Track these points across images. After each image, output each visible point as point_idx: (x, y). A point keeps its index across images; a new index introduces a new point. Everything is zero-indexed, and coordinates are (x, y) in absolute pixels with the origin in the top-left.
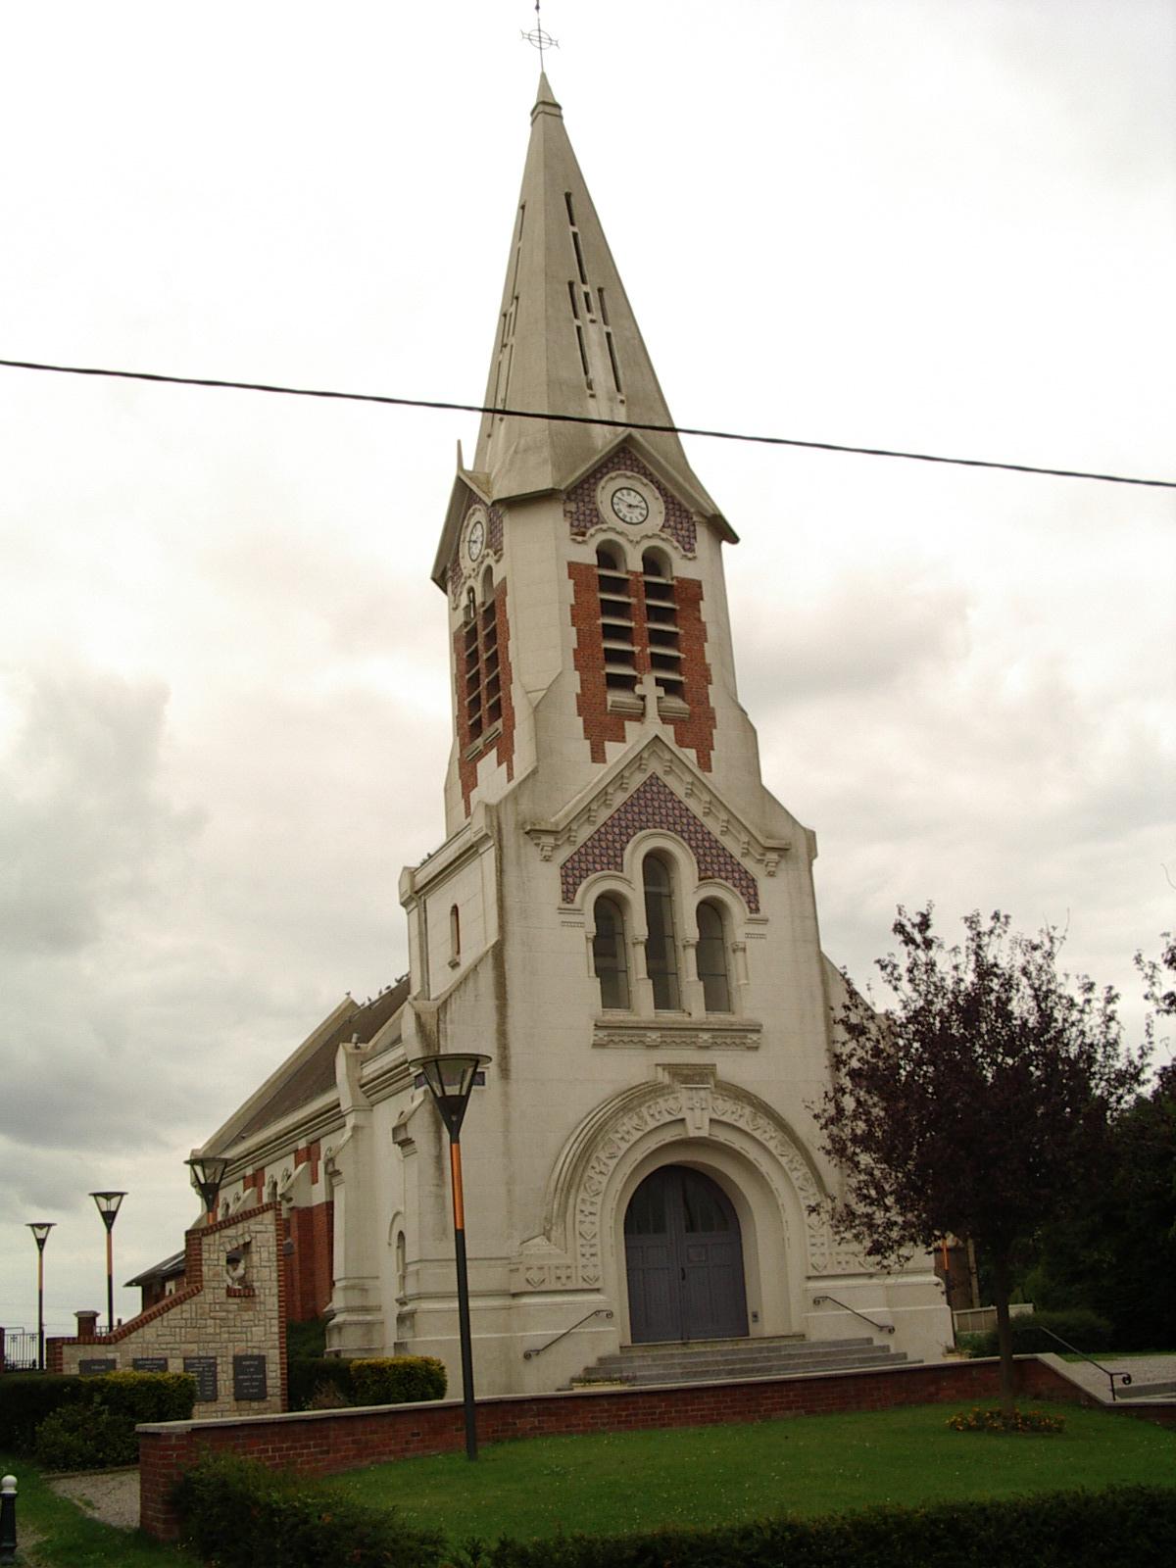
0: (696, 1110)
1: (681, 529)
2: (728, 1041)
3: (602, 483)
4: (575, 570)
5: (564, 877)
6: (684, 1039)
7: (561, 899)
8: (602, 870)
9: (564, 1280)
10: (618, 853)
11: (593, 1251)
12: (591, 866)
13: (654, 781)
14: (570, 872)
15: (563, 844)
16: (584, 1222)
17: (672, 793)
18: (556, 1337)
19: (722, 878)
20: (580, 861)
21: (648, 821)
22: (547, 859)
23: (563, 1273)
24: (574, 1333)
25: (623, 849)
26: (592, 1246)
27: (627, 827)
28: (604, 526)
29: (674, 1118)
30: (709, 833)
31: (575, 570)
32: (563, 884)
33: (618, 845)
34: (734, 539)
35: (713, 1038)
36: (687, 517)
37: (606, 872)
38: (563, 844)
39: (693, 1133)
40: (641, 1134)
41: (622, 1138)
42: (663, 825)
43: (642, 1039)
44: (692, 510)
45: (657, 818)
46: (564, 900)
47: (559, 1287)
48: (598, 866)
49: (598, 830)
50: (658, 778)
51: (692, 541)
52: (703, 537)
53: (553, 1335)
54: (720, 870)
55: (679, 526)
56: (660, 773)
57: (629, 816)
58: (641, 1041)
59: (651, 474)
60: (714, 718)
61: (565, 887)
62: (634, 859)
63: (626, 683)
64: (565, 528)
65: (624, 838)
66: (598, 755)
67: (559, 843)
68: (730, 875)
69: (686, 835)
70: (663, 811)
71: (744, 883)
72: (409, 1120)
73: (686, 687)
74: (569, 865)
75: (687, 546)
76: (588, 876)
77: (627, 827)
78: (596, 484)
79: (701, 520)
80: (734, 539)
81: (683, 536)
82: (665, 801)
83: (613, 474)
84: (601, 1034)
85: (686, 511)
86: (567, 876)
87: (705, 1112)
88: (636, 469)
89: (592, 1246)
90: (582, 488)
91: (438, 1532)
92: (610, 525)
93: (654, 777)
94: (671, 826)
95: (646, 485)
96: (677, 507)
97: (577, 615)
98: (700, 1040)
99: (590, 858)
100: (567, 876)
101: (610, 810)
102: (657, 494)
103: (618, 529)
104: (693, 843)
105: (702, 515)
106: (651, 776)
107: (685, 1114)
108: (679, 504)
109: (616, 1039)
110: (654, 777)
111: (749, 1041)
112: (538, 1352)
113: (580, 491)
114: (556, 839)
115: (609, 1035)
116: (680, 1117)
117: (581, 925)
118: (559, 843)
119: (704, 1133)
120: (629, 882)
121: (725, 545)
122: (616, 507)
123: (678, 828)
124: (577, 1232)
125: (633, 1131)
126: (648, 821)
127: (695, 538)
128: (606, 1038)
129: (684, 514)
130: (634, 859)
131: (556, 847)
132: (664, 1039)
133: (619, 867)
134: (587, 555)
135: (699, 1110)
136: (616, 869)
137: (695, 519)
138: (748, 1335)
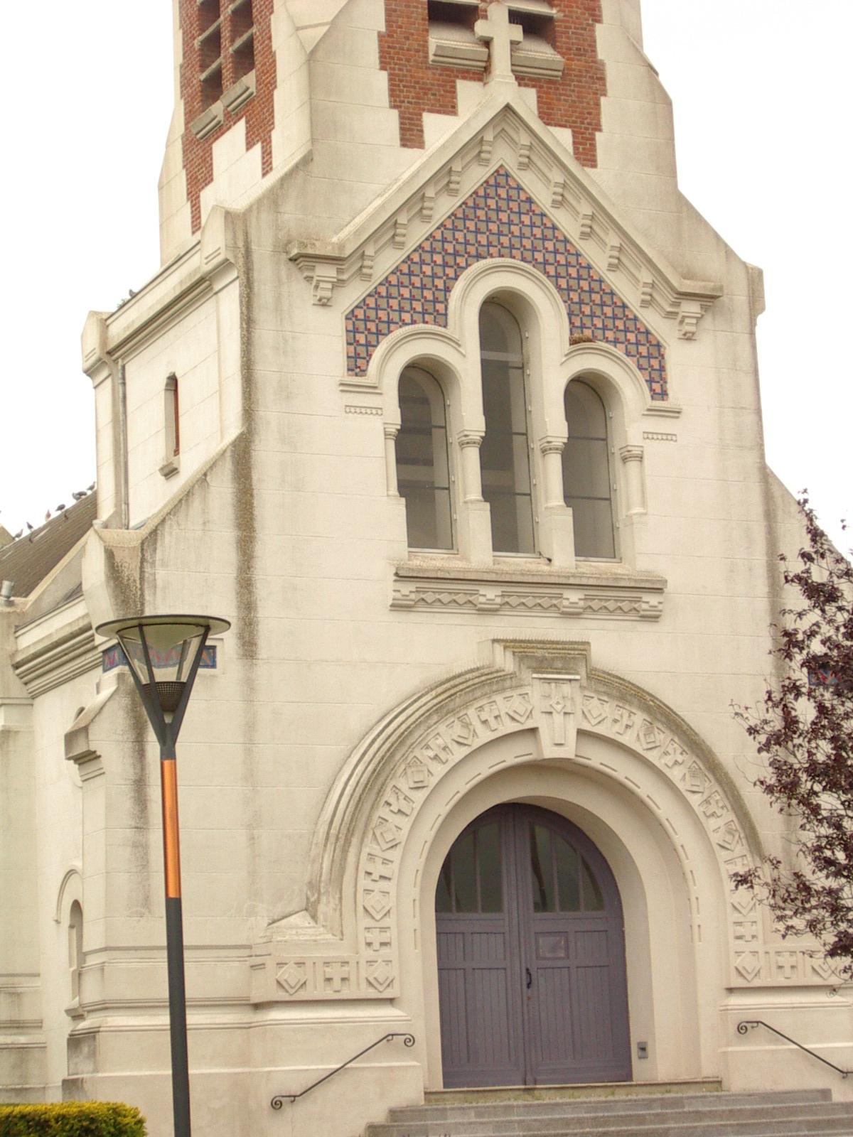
8: (413, 322)
9: (337, 983)
11: (385, 937)
13: (502, 180)
17: (530, 200)
19: (607, 341)
20: (377, 308)
22: (324, 303)
23: (336, 972)
24: (352, 1068)
25: (447, 290)
27: (456, 254)
30: (589, 267)
32: (349, 344)
33: (440, 283)
40: (465, 751)
41: (436, 757)
47: (330, 995)
50: (507, 175)
60: (602, 79)
66: (411, 135)
67: (345, 277)
69: (551, 269)
82: (520, 213)
84: (407, 588)
86: (356, 331)
93: (501, 174)
94: (528, 255)
100: (356, 331)
104: (563, 283)
106: (497, 171)
110: (501, 174)
112: (293, 1098)
114: (340, 271)
116: (529, 725)
117: (378, 410)
118: (345, 277)
120: (455, 343)
123: (540, 258)
131: (339, 284)
133: (441, 318)
136: (436, 322)
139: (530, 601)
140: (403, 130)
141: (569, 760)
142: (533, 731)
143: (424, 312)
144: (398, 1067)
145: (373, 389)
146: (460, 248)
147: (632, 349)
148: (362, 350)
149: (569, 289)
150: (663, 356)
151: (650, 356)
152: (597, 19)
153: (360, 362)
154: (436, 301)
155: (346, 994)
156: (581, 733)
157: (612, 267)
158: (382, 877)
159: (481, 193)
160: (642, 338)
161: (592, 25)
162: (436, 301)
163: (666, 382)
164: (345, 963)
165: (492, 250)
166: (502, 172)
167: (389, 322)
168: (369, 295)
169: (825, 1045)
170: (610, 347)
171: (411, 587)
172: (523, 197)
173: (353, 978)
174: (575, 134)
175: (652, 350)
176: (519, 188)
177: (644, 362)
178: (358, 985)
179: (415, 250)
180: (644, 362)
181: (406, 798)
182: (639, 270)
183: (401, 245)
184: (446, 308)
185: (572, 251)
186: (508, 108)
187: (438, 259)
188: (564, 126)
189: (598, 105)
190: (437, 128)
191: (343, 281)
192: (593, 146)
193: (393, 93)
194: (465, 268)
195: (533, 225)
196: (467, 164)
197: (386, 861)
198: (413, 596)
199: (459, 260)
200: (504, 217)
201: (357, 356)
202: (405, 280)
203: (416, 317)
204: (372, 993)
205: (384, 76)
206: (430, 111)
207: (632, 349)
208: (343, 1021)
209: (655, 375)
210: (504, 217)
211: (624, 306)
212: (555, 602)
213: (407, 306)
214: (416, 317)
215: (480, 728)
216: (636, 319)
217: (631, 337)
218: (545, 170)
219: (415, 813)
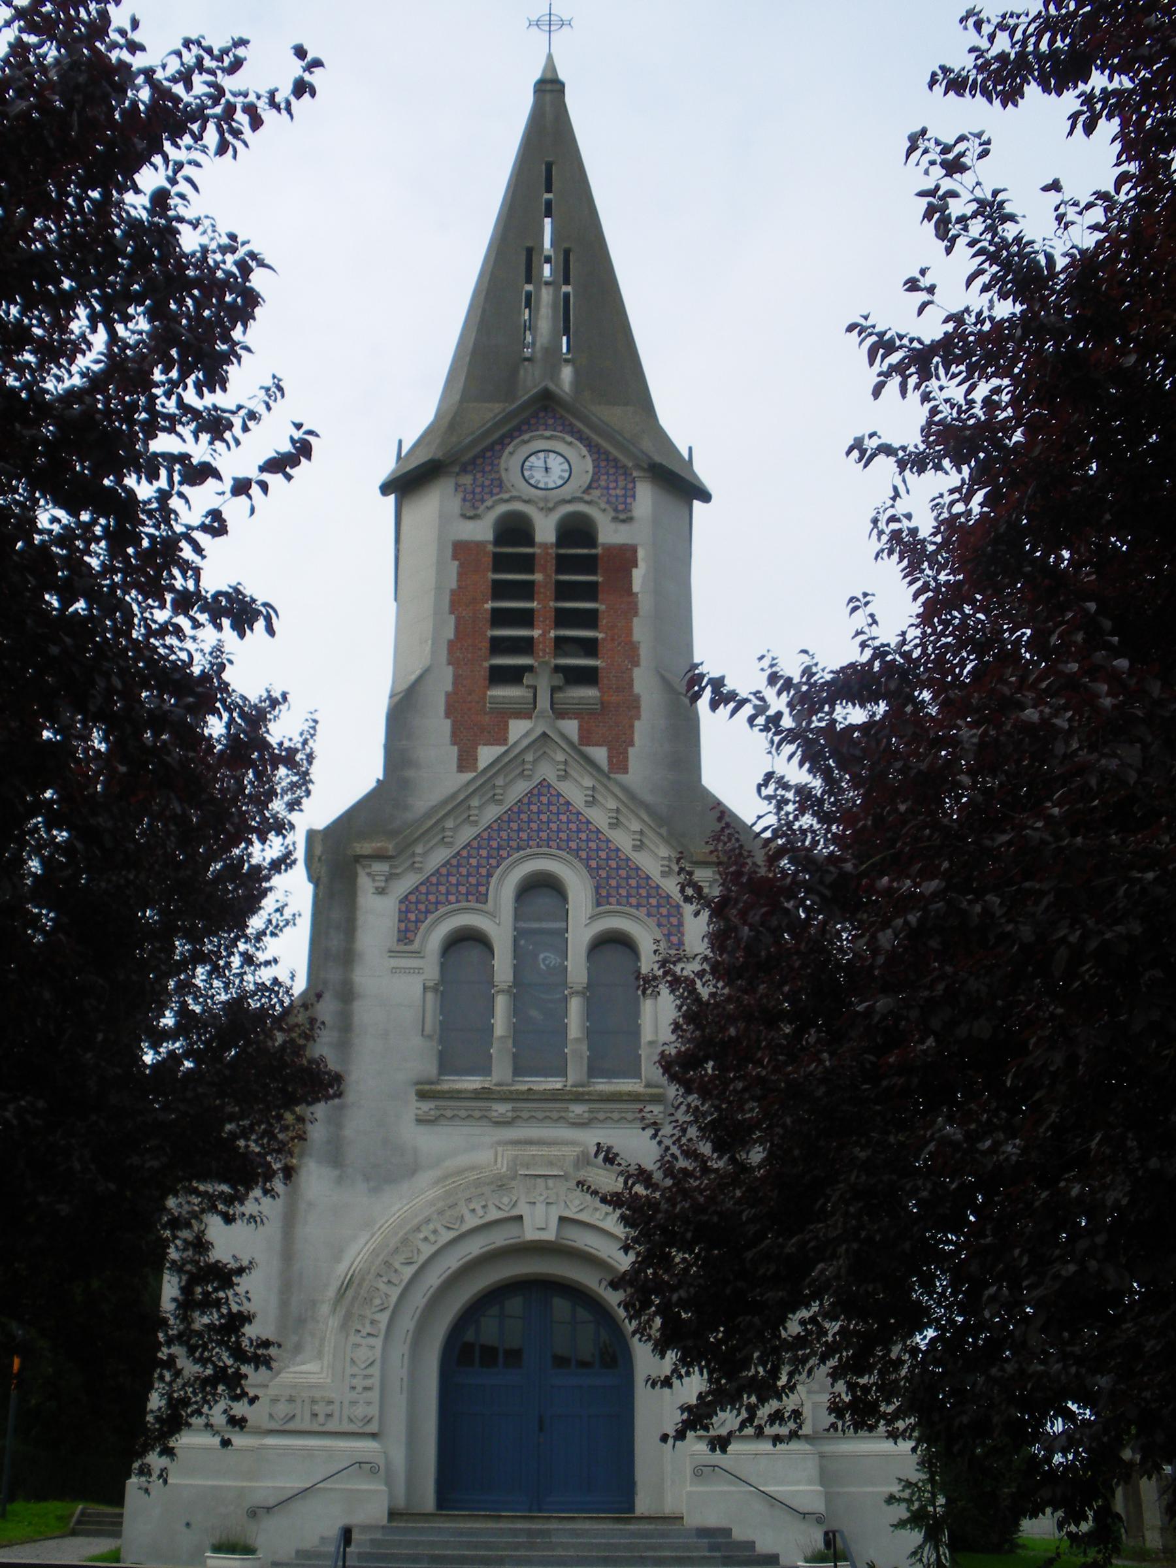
0: (538, 1205)
1: (615, 489)
2: (616, 1116)
3: (510, 448)
4: (461, 550)
5: (403, 916)
6: (548, 1114)
7: (395, 939)
8: (458, 901)
9: (321, 1418)
10: (484, 881)
11: (368, 1383)
12: (442, 898)
13: (545, 790)
14: (413, 907)
15: (403, 872)
16: (359, 1345)
17: (568, 803)
18: (296, 1492)
19: (631, 906)
20: (428, 893)
21: (530, 838)
22: (381, 891)
23: (320, 1409)
24: (325, 1489)
25: (490, 875)
26: (366, 1377)
27: (500, 848)
28: (506, 496)
29: (505, 1215)
30: (618, 850)
31: (461, 550)
32: (400, 921)
33: (483, 871)
34: (706, 497)
35: (590, 1111)
36: (625, 474)
37: (464, 904)
38: (403, 872)
39: (530, 1234)
40: (452, 1235)
41: (426, 1239)
42: (551, 843)
43: (563, 1114)
44: (630, 464)
45: (544, 835)
46: (399, 940)
47: (315, 1427)
48: (452, 898)
49: (458, 853)
50: (549, 786)
51: (629, 500)
52: (645, 498)
53: (292, 1488)
54: (629, 896)
55: (612, 485)
56: (552, 779)
57: (504, 835)
58: (561, 1117)
59: (588, 438)
60: (638, 708)
61: (403, 925)
62: (505, 889)
63: (513, 676)
64: (455, 504)
65: (493, 862)
66: (466, 761)
67: (398, 871)
68: (644, 901)
69: (583, 855)
70: (554, 826)
71: (664, 911)
72: (595, 1193)
73: (602, 674)
74: (413, 898)
75: (621, 507)
76: (437, 910)
77: (500, 848)
78: (502, 450)
79: (642, 474)
80: (706, 497)
81: (617, 496)
82: (558, 814)
83: (526, 437)
84: (426, 1106)
85: (624, 467)
86: (408, 911)
87: (553, 1209)
88: (560, 428)
89: (366, 1377)
90: (484, 457)
91: (900, 1500)
92: (515, 493)
93: (543, 783)
94: (563, 845)
95: (570, 444)
96: (612, 464)
97: (457, 601)
98: (571, 1115)
99: (443, 889)
100: (408, 911)
101: (475, 829)
102: (584, 451)
103: (525, 497)
104: (593, 864)
105: (638, 467)
106: (540, 783)
107: (522, 1209)
108: (615, 460)
109: (449, 1113)
110: (543, 783)
111: (571, 1115)
112: (268, 1509)
113: (479, 461)
114: (391, 867)
115: (437, 1108)
116: (515, 1212)
117: (419, 971)
118: (398, 871)
119: (550, 1235)
120: (492, 915)
121: (697, 504)
122: (532, 481)
123: (573, 845)
124: (348, 1359)
125: (443, 1231)
126: (530, 838)
127: (634, 496)
128: (432, 1113)
129: (603, 457)
130: (505, 889)
131: (391, 877)
132: (595, 1115)
133: (483, 898)
134: (482, 531)
135: (544, 1205)
136: (477, 901)
137: (635, 474)
138: (631, 1509)
139: (540, 1115)
140: (461, 759)
141: (551, 1242)
142: (520, 1218)
143: (468, 893)
144: (558, 1529)
145: (417, 954)
146: (504, 843)
147: (654, 911)
148: (412, 926)
149: (599, 868)
150: (682, 915)
151: (669, 915)
152: (637, 664)
153: (409, 935)
154: (479, 884)
155: (332, 1426)
156: (562, 1220)
157: (636, 848)
158: (369, 1334)
159: (526, 800)
160: (663, 901)
161: (631, 670)
162: (479, 884)
163: (683, 935)
164: (330, 1402)
165: (531, 843)
166: (545, 784)
167: (438, 903)
168: (421, 884)
169: (777, 1488)
170: (633, 911)
171: (431, 1105)
172: (562, 801)
173: (336, 1414)
174: (610, 750)
175: (672, 910)
176: (559, 795)
177: (664, 921)
178: (340, 1421)
179: (464, 848)
180: (664, 921)
181: (396, 1271)
182: (657, 847)
183: (450, 845)
184: (487, 890)
185: (603, 838)
186: (544, 734)
187: (484, 853)
188: (601, 745)
189: (632, 726)
190: (487, 754)
191: (397, 874)
192: (626, 759)
193: (454, 734)
194: (505, 859)
195: (569, 821)
196: (511, 781)
197: (373, 1322)
198: (432, 1113)
199: (501, 852)
200: (544, 817)
201: (407, 930)
202: (454, 870)
203: (460, 897)
204: (352, 1428)
205: (448, 722)
206: (485, 745)
207: (654, 911)
208: (287, 1448)
209: (674, 930)
210: (544, 817)
211: (648, 878)
212: (563, 1114)
213: (453, 890)
214: (460, 897)
215: (468, 1216)
216: (658, 887)
217: (653, 901)
218: (579, 779)
219: (403, 1284)
